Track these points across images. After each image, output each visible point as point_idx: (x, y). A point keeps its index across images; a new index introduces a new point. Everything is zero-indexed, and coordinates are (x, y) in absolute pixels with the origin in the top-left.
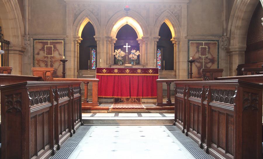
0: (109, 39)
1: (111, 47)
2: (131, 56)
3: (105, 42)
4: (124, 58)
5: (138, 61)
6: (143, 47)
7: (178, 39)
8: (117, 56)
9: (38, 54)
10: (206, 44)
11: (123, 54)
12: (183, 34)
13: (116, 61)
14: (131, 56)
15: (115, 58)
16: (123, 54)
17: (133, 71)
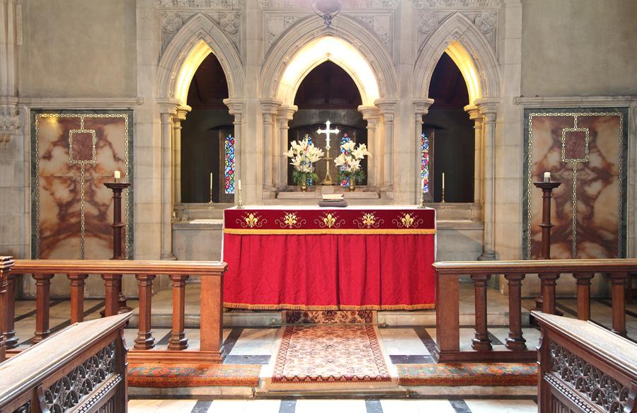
0: (271, 107)
1: (280, 132)
2: (339, 161)
3: (259, 119)
4: (319, 166)
5: (361, 178)
6: (377, 133)
7: (491, 106)
8: (296, 162)
9: (48, 157)
10: (583, 121)
11: (314, 153)
12: (509, 92)
13: (293, 178)
14: (339, 161)
15: (291, 168)
16: (314, 153)
17: (350, 219)
